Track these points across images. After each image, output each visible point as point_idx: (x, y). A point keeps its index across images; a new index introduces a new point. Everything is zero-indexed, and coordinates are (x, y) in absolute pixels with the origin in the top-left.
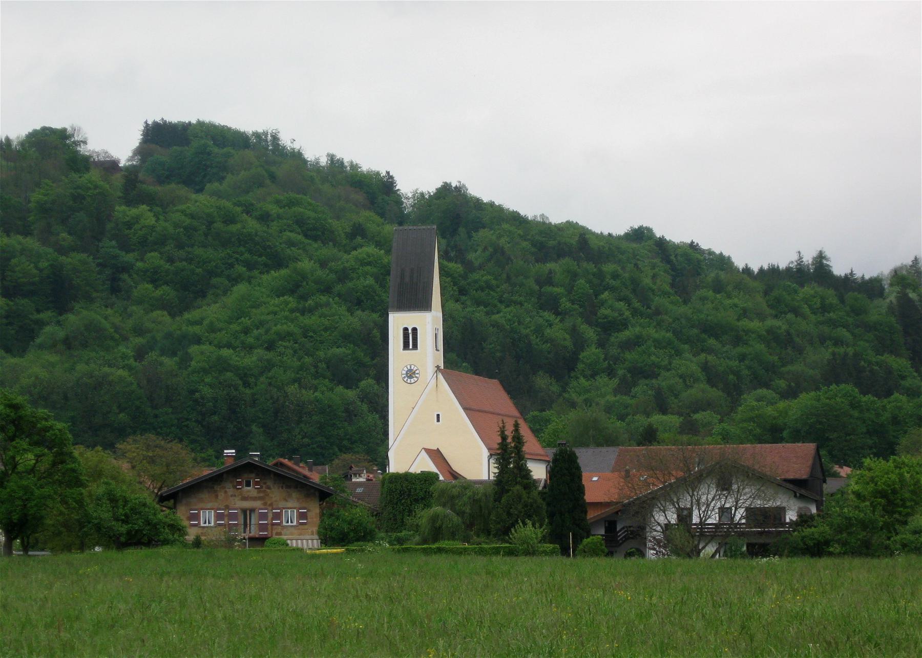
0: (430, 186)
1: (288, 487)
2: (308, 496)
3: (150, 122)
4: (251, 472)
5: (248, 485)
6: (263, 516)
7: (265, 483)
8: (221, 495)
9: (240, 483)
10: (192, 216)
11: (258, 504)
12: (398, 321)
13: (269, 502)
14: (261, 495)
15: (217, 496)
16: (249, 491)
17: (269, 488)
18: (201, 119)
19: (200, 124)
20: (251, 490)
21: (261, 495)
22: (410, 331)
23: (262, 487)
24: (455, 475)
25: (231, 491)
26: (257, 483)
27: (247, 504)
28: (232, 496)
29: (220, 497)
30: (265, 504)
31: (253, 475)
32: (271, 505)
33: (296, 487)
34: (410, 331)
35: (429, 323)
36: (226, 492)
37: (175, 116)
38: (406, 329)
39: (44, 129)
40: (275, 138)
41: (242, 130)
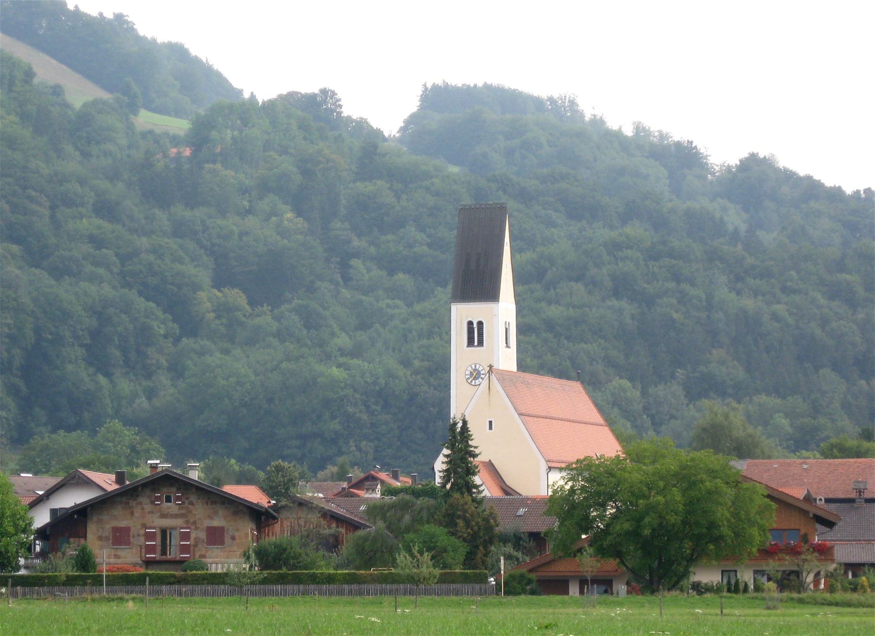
0: (734, 160)
1: (214, 503)
2: (236, 513)
3: (429, 86)
4: (172, 485)
5: (168, 500)
6: (185, 536)
7: (187, 498)
8: (137, 513)
9: (158, 499)
10: (437, 194)
11: (179, 522)
12: (461, 314)
13: (191, 521)
14: (183, 511)
15: (132, 514)
16: (168, 508)
17: (192, 504)
18: (489, 82)
19: (487, 87)
20: (172, 507)
21: (183, 511)
22: (475, 325)
23: (183, 503)
24: (507, 490)
25: (148, 507)
26: (178, 499)
27: (166, 523)
28: (149, 513)
29: (137, 514)
30: (187, 522)
31: (174, 489)
32: (195, 523)
33: (223, 503)
34: (475, 325)
35: (502, 313)
36: (143, 509)
37: (457, 79)
38: (470, 323)
39: (291, 95)
40: (572, 103)
41: (536, 94)
